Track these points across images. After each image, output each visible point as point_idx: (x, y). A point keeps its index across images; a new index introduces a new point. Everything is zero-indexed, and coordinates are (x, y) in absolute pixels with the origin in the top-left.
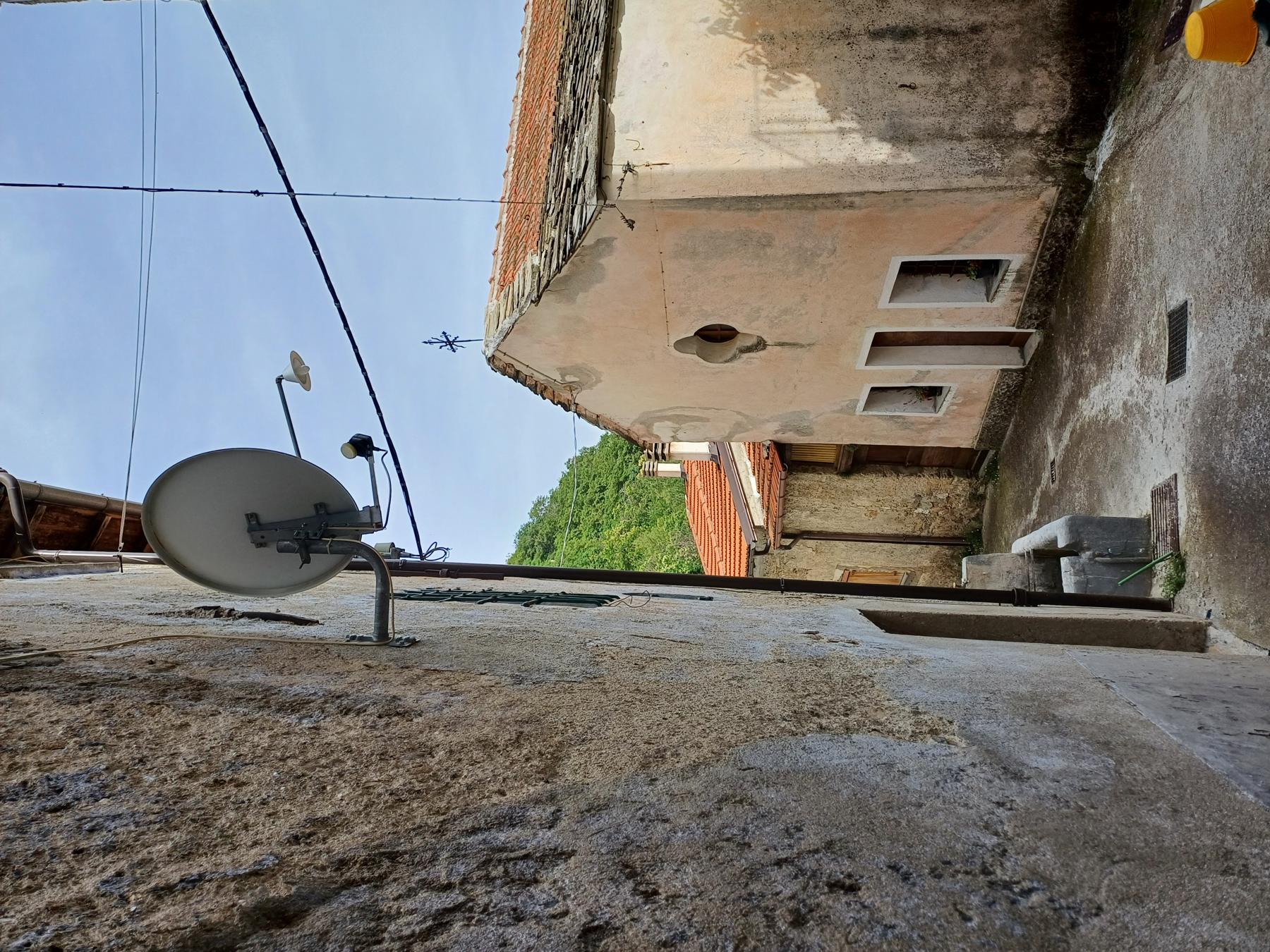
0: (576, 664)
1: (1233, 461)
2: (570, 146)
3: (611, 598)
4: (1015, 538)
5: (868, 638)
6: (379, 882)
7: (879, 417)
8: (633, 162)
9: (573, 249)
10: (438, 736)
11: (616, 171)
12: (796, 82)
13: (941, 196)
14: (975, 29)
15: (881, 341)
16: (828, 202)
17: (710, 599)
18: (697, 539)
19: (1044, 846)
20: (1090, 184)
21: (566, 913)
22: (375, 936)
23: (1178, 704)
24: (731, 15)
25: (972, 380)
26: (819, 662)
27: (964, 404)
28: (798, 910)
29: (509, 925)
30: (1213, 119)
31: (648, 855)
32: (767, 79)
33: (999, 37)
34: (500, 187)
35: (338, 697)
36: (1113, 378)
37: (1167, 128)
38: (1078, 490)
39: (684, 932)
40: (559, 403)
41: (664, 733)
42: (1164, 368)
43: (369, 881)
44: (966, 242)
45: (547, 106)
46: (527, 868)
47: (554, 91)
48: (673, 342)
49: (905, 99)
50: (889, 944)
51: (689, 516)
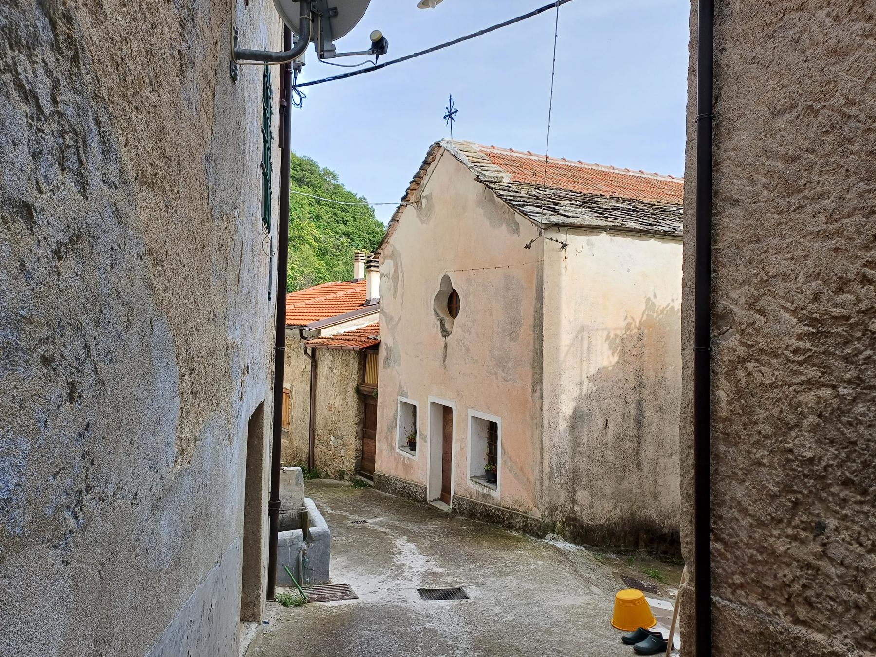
0: (222, 202)
1: (367, 632)
2: (580, 206)
3: (268, 228)
4: (315, 500)
5: (245, 407)
6: (55, 47)
7: (396, 411)
8: (568, 248)
9: (512, 206)
10: (166, 97)
11: (563, 237)
12: (613, 354)
13: (538, 446)
14: (639, 465)
15: (447, 411)
16: (537, 376)
17: (269, 299)
18: (311, 289)
19: (108, 526)
20: (542, 537)
21: (41, 192)
22: (15, 44)
23: (207, 607)
24: (657, 312)
25: (420, 469)
26: (228, 374)
27: (404, 464)
28: (54, 360)
29: (29, 149)
30: (579, 607)
31: (87, 252)
32: (616, 336)
33: (634, 479)
34: (555, 156)
35: (193, 19)
36: (421, 557)
37: (574, 581)
38: (347, 538)
39: (33, 279)
40: (407, 194)
41: (175, 265)
42: (427, 587)
43: (56, 40)
44: (509, 463)
45: (607, 191)
46: (72, 162)
47: (616, 195)
48: (450, 274)
49: (599, 423)
50: (34, 425)
51: (327, 284)
